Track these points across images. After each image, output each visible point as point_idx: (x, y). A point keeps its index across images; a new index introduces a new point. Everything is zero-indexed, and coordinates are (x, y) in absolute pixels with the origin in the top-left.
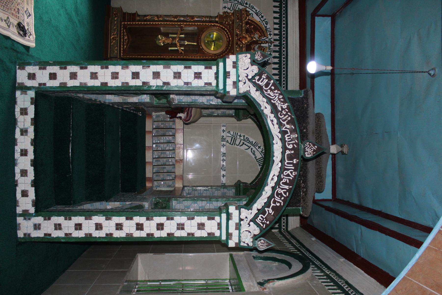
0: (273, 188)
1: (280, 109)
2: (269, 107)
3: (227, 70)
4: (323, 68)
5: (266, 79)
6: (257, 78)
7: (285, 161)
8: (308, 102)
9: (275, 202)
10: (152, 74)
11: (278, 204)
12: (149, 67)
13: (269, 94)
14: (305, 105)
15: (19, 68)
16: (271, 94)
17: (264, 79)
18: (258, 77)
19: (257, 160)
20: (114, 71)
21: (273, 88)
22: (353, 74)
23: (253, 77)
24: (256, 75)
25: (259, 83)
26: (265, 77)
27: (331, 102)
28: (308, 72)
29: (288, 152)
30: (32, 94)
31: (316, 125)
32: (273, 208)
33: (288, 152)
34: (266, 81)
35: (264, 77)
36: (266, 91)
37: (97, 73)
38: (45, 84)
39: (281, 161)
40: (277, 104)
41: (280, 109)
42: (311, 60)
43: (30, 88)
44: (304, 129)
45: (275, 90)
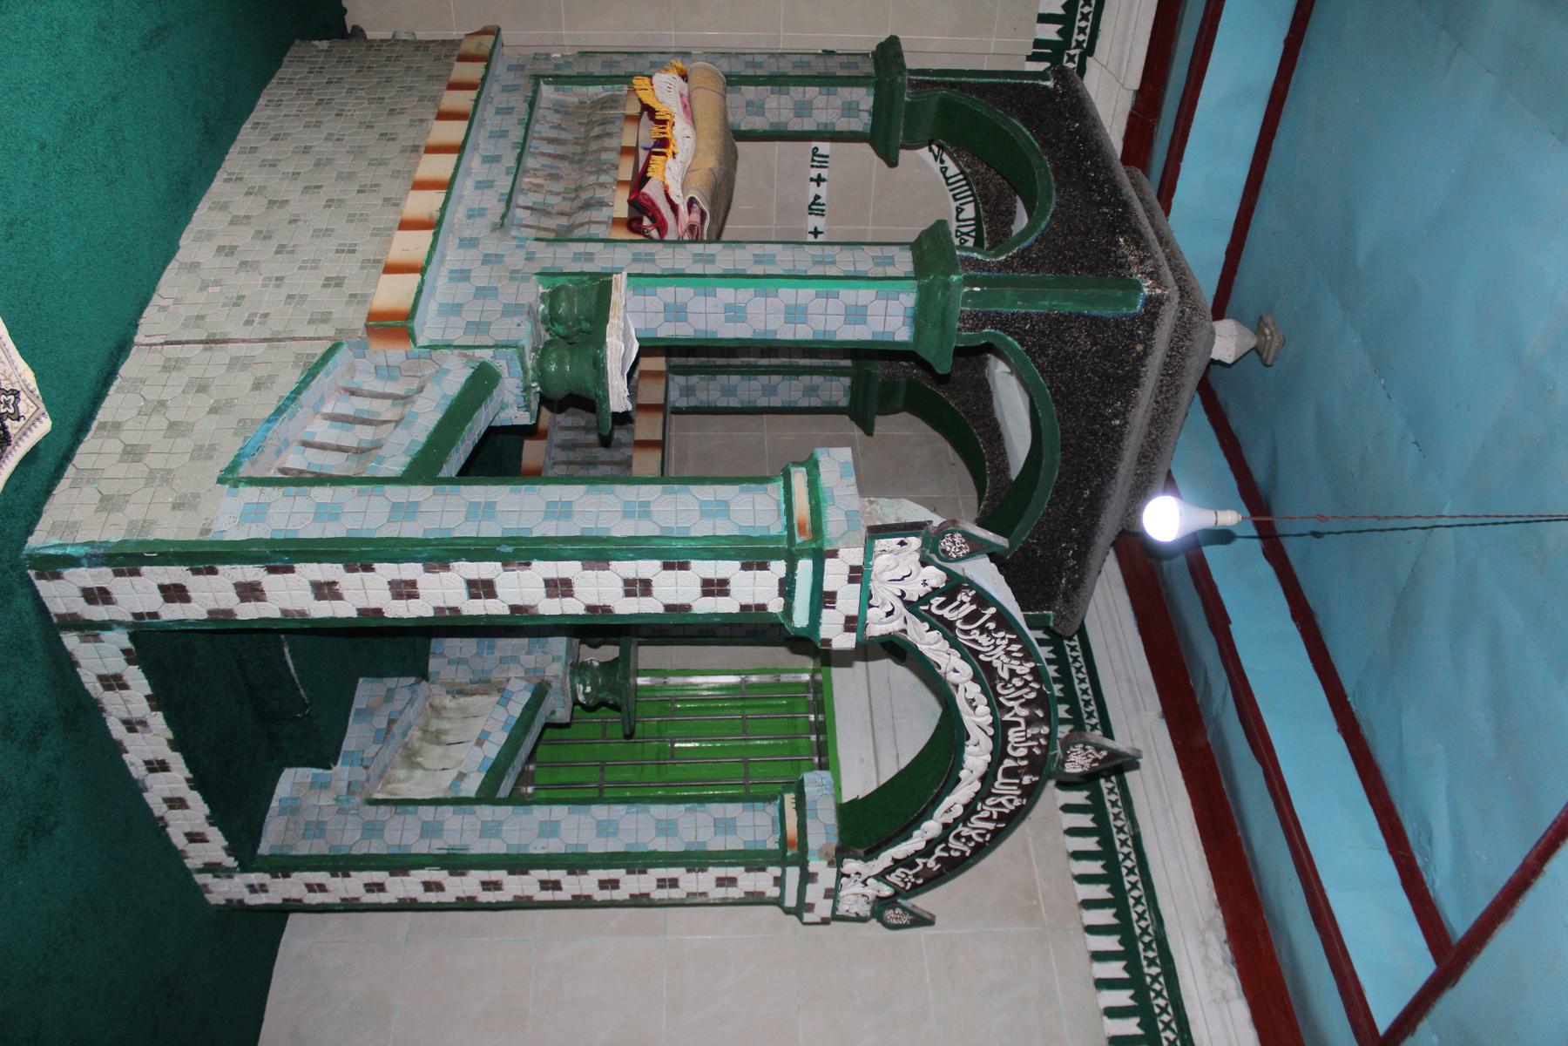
0: (947, 827)
1: (1005, 675)
2: (966, 670)
3: (827, 587)
4: (1206, 519)
5: (971, 603)
6: (937, 601)
7: (996, 779)
8: (1151, 339)
9: (947, 849)
10: (543, 584)
11: (954, 854)
12: (528, 564)
13: (975, 641)
14: (1139, 348)
15: (40, 576)
16: (984, 639)
17: (962, 603)
18: (942, 599)
19: (947, 179)
20: (397, 577)
21: (992, 626)
22: (1316, 534)
23: (925, 599)
24: (935, 591)
25: (946, 613)
26: (966, 599)
27: (1288, 41)
28: (1140, 518)
29: (1008, 763)
30: (121, 639)
31: (1172, 349)
32: (939, 860)
33: (1008, 763)
34: (968, 609)
35: (962, 597)
36: (967, 632)
37: (334, 583)
38: (154, 615)
39: (983, 779)
40: (997, 664)
41: (1005, 675)
42: (1165, 491)
43: (106, 626)
44: (1116, 416)
45: (997, 630)
